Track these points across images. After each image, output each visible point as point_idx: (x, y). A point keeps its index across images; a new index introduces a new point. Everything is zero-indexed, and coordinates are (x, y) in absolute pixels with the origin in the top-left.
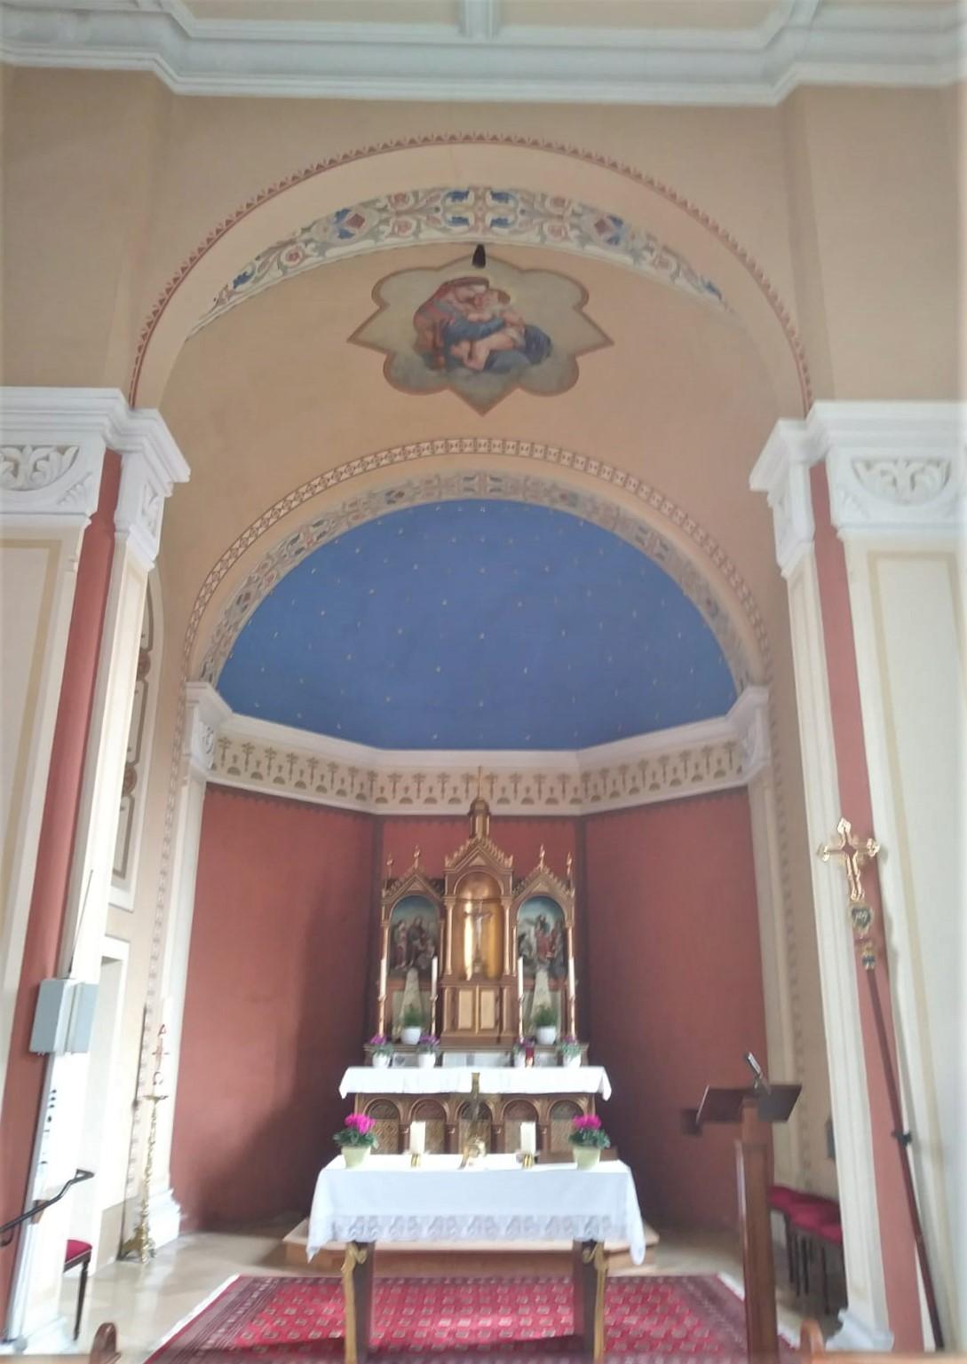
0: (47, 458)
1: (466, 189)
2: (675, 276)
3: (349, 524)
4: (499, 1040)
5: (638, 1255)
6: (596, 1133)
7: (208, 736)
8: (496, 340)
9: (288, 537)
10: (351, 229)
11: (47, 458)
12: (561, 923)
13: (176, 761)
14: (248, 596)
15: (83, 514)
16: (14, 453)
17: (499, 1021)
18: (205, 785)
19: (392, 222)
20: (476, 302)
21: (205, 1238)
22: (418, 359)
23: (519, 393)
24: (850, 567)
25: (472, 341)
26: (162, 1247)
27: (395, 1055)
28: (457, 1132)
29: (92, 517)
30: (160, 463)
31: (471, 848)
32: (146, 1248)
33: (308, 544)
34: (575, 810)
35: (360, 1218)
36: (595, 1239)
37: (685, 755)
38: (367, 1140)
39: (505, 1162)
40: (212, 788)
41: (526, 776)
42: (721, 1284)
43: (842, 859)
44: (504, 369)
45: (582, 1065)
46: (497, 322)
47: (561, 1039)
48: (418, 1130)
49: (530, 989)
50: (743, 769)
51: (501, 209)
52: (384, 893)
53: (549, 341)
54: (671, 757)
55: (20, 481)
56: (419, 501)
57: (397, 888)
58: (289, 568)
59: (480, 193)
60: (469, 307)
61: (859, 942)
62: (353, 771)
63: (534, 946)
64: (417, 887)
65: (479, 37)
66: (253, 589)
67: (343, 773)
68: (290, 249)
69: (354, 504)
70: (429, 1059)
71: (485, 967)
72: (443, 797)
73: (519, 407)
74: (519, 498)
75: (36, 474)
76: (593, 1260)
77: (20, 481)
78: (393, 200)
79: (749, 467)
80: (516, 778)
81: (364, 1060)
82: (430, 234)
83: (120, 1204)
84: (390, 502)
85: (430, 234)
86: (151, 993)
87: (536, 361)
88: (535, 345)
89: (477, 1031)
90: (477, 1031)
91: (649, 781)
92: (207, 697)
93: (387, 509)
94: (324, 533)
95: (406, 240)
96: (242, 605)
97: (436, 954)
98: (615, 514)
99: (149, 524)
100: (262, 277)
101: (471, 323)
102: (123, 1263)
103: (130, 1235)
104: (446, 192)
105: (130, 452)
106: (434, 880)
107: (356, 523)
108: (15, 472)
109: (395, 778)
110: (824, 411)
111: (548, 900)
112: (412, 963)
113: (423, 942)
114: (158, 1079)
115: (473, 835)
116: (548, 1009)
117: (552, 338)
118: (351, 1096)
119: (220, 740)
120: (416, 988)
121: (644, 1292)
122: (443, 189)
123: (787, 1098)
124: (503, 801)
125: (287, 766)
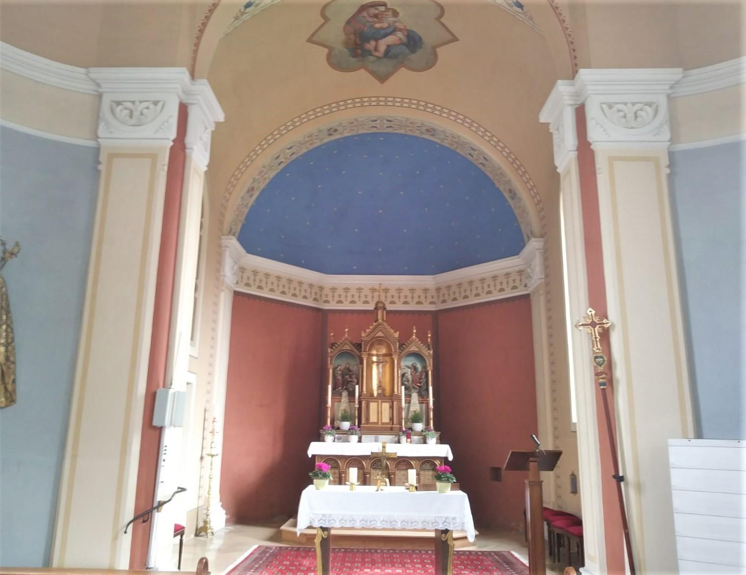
0: (148, 108)
4: (392, 429)
5: (471, 539)
6: (449, 475)
7: (234, 266)
8: (390, 40)
11: (148, 108)
12: (425, 367)
13: (217, 279)
15: (168, 139)
16: (129, 105)
17: (392, 419)
18: (233, 292)
20: (380, 16)
21: (239, 527)
23: (403, 71)
24: (598, 166)
25: (377, 40)
26: (218, 531)
27: (337, 436)
28: (370, 476)
29: (174, 141)
30: (208, 113)
31: (376, 327)
32: (209, 531)
34: (432, 308)
35: (324, 515)
36: (448, 528)
37: (495, 278)
38: (327, 475)
39: (399, 489)
40: (236, 294)
41: (407, 289)
42: (513, 555)
43: (589, 329)
44: (395, 57)
45: (437, 443)
46: (391, 29)
47: (426, 429)
48: (353, 472)
49: (408, 402)
50: (528, 285)
52: (329, 350)
53: (420, 38)
54: (486, 279)
55: (134, 121)
56: (346, 134)
57: (337, 348)
58: (275, 173)
61: (597, 374)
63: (410, 380)
64: (347, 347)
67: (305, 287)
69: (310, 136)
70: (354, 438)
71: (384, 390)
72: (359, 300)
73: (403, 79)
74: (402, 132)
76: (447, 539)
79: (541, 105)
80: (399, 290)
81: (320, 438)
83: (195, 509)
84: (330, 135)
86: (208, 401)
87: (413, 51)
88: (413, 42)
89: (380, 423)
90: (380, 423)
93: (328, 139)
96: (250, 194)
97: (357, 384)
102: (198, 538)
103: (201, 524)
105: (192, 104)
106: (356, 343)
107: (311, 147)
108: (131, 116)
109: (333, 289)
110: (584, 74)
111: (418, 355)
112: (345, 387)
113: (351, 377)
114: (213, 445)
115: (377, 320)
116: (419, 413)
117: (422, 37)
118: (314, 456)
119: (240, 268)
120: (347, 401)
121: (472, 559)
123: (552, 459)
124: (393, 303)
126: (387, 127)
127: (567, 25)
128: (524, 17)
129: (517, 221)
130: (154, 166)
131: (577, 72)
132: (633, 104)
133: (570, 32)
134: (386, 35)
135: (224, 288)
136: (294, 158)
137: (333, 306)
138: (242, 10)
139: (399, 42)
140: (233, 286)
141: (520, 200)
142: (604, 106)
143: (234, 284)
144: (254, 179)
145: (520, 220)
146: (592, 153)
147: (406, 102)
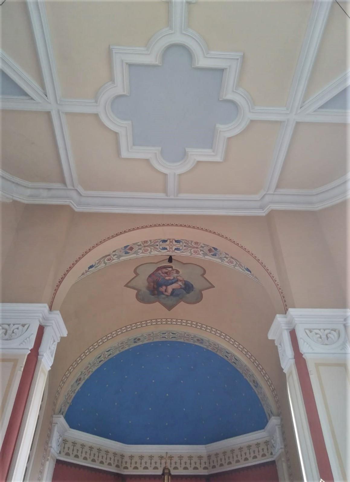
0: (18, 329)
1: (166, 239)
2: (235, 266)
3: (119, 351)
7: (59, 438)
8: (175, 286)
9: (98, 356)
10: (129, 251)
11: (18, 329)
13: (46, 450)
14: (80, 379)
15: (28, 349)
16: (6, 327)
19: (142, 249)
20: (168, 273)
22: (148, 292)
30: (58, 329)
33: (104, 358)
40: (58, 462)
44: (177, 295)
50: (273, 453)
51: (178, 245)
53: (193, 285)
55: (7, 337)
58: (96, 368)
59: (171, 240)
60: (166, 275)
62: (115, 454)
65: (172, 197)
66: (82, 377)
68: (108, 257)
73: (182, 308)
74: (182, 340)
75: (13, 334)
77: (7, 337)
78: (143, 242)
80: (181, 457)
82: (154, 253)
84: (135, 342)
85: (154, 253)
87: (188, 293)
88: (188, 287)
91: (235, 459)
92: (61, 421)
94: (111, 354)
95: (147, 254)
96: (78, 382)
98: (217, 346)
99: (51, 352)
100: (98, 266)
101: (166, 280)
104: (161, 240)
107: (122, 350)
108: (5, 334)
110: (292, 311)
119: (64, 440)
122: (159, 239)
124: (176, 468)
125: (89, 452)
126: (172, 337)
127: (278, 282)
128: (252, 277)
129: (260, 403)
130: (15, 366)
131: (287, 310)
132: (324, 330)
133: (280, 286)
134: (172, 283)
135: (49, 458)
136: (110, 358)
137: (130, 472)
138: (87, 270)
139: (180, 287)
140: (56, 455)
141: (261, 388)
142: (307, 331)
143: (57, 453)
144: (82, 372)
145: (262, 403)
146: (304, 361)
147: (183, 322)
